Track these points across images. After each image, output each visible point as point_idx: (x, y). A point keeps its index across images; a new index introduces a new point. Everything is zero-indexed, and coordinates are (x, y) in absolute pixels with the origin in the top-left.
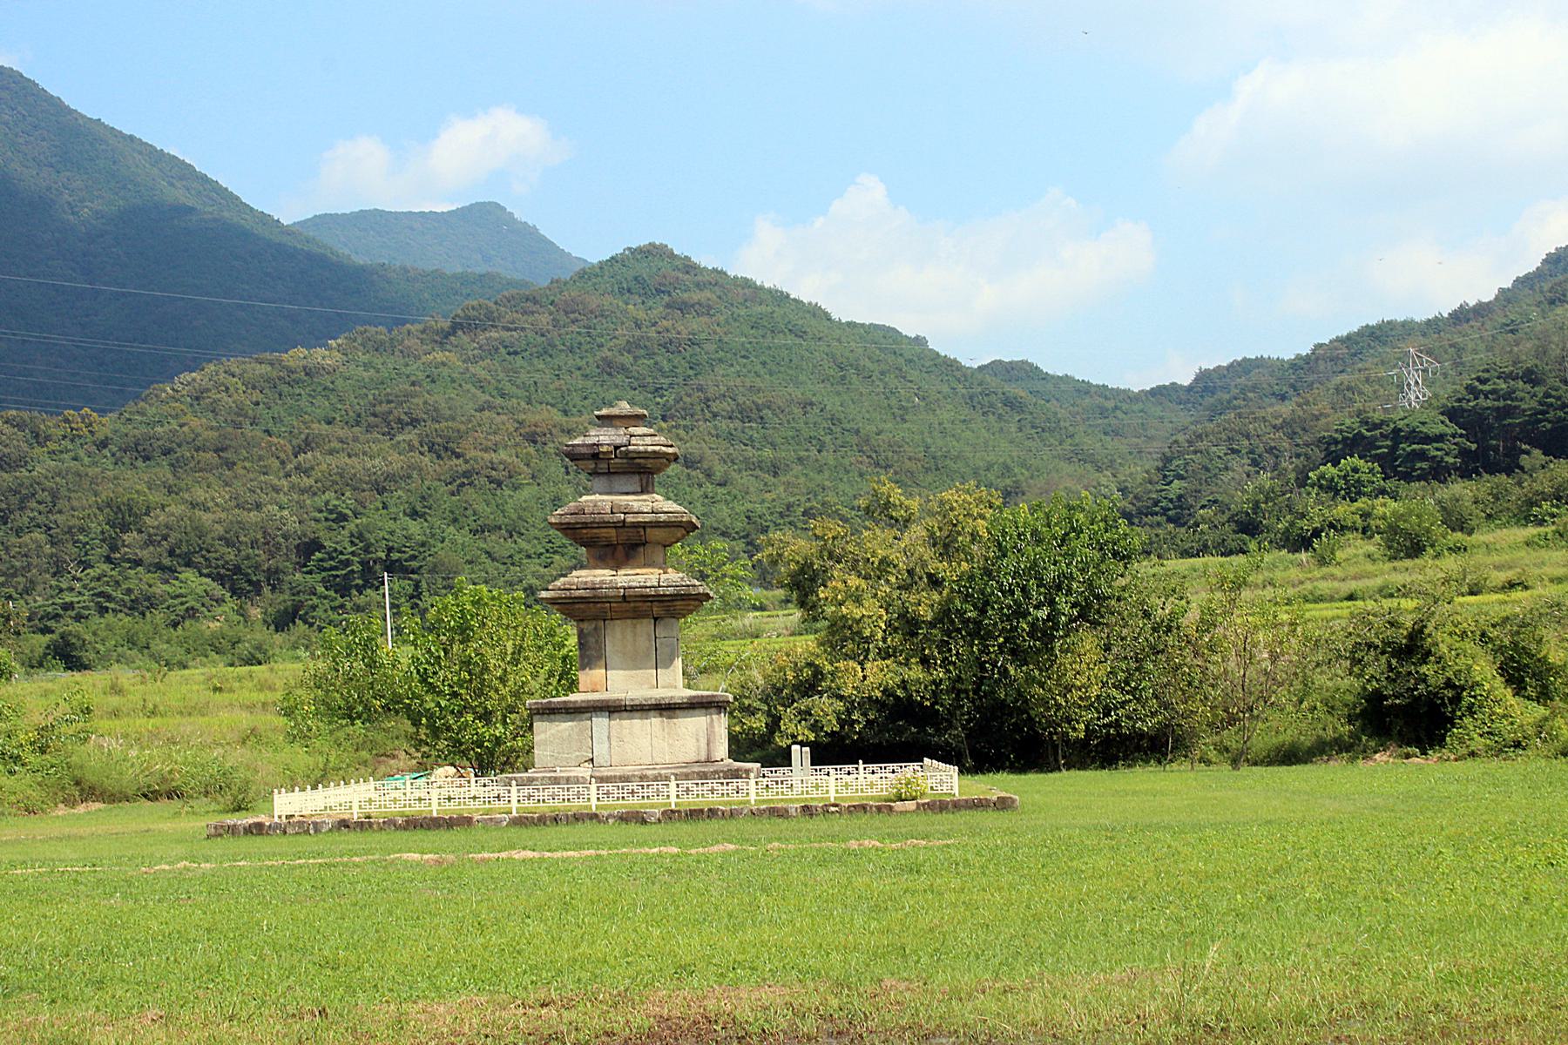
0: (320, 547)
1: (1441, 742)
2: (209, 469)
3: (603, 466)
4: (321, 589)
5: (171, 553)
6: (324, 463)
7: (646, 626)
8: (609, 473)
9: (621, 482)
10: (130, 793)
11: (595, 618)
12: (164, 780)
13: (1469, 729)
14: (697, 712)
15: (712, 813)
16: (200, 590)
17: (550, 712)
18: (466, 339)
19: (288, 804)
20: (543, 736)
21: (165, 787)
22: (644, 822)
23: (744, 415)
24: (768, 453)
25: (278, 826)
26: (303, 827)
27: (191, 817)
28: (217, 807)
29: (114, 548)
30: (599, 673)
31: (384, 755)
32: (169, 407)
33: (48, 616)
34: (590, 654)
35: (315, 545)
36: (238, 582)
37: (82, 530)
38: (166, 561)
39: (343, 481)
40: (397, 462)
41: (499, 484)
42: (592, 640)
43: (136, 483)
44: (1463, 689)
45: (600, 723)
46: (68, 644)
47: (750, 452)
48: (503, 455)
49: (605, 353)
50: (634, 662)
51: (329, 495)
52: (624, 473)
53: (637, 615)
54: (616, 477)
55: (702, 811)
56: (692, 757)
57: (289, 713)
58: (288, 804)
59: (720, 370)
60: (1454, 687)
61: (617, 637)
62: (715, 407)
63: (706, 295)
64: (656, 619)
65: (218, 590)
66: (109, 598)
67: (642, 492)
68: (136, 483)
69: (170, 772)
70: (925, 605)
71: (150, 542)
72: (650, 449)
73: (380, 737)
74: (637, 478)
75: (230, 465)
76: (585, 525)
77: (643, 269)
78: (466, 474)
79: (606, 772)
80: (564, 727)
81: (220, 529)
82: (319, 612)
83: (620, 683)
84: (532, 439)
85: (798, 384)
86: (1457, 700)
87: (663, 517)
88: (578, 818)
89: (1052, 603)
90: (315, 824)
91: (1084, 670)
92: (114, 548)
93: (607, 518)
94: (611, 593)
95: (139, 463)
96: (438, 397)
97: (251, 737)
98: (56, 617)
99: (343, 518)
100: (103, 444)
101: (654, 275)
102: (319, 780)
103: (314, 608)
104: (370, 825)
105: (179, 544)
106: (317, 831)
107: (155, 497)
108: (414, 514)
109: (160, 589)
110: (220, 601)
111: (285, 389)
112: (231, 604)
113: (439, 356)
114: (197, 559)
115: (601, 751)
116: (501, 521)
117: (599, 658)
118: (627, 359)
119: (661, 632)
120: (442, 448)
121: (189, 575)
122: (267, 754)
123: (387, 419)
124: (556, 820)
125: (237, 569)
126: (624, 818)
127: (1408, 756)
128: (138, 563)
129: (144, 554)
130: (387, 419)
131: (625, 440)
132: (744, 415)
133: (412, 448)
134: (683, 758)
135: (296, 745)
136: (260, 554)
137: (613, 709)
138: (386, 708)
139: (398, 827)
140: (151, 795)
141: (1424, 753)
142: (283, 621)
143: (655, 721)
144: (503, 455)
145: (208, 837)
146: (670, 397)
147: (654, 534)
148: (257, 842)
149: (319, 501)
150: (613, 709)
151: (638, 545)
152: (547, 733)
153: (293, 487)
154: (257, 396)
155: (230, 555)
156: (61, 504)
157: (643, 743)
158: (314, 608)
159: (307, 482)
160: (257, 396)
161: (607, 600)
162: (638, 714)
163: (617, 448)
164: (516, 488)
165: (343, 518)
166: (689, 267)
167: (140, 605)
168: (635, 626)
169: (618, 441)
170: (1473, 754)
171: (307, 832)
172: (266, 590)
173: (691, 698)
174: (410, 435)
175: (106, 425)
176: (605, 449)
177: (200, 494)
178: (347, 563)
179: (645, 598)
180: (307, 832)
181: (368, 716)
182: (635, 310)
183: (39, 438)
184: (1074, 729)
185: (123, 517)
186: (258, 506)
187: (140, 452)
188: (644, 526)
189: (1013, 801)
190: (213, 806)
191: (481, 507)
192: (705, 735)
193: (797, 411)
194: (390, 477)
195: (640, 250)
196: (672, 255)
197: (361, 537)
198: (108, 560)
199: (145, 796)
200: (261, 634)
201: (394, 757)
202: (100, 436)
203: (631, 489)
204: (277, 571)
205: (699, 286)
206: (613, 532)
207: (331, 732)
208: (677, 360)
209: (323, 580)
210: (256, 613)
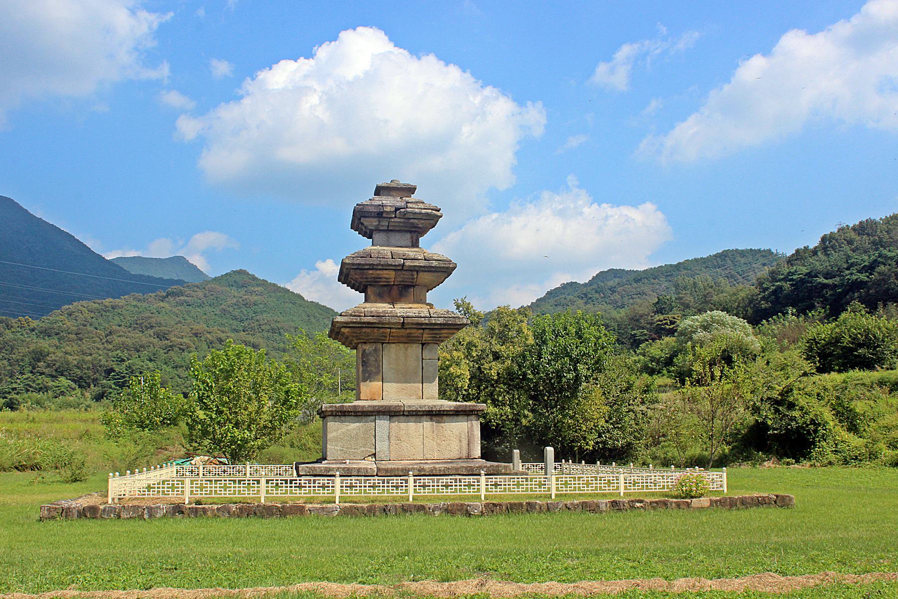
0: (114, 371)
1: (806, 456)
2: (73, 341)
3: (385, 223)
4: (113, 386)
5: (56, 371)
6: (117, 340)
7: (415, 350)
8: (388, 231)
9: (396, 237)
10: (6, 466)
11: (376, 341)
12: (29, 458)
13: (826, 447)
14: (460, 418)
15: (531, 507)
16: (66, 385)
17: (342, 414)
18: (172, 299)
19: (122, 487)
20: (334, 434)
21: (29, 463)
22: (469, 514)
23: (273, 331)
24: (282, 345)
25: (112, 510)
26: (137, 512)
27: (41, 486)
28: (58, 478)
29: (34, 368)
30: (376, 385)
31: (161, 448)
32: (57, 318)
33: (6, 392)
34: (369, 369)
35: (112, 370)
36: (82, 383)
37: (22, 360)
38: (54, 373)
39: (124, 347)
40: (145, 340)
41: (183, 350)
42: (372, 359)
43: (45, 344)
44: (819, 424)
45: (382, 424)
46: (12, 403)
47: (275, 344)
48: (185, 340)
49: (223, 306)
50: (404, 377)
51: (118, 352)
52: (399, 231)
53: (409, 340)
54: (393, 234)
55: (521, 504)
56: (455, 454)
57: (108, 423)
58: (122, 487)
59: (265, 315)
60: (815, 424)
61: (392, 356)
62: (263, 327)
63: (260, 289)
64: (423, 344)
65: (73, 385)
66: (31, 387)
67: (413, 246)
68: (45, 344)
69: (34, 454)
70: (494, 369)
71: (48, 366)
72: (424, 211)
73: (158, 438)
74: (408, 236)
75: (81, 340)
76: (373, 267)
77: (238, 278)
78: (171, 346)
79: (384, 465)
80: (353, 426)
81: (76, 362)
82: (112, 395)
83: (393, 394)
84: (196, 335)
85: (293, 321)
86: (816, 431)
87: (435, 263)
88: (405, 509)
89: (575, 369)
90: (150, 509)
91: (593, 407)
92: (34, 368)
93: (390, 261)
94: (393, 320)
95: (46, 338)
96: (160, 318)
97: (86, 435)
98: (9, 393)
99: (123, 360)
100: (33, 330)
101: (240, 280)
102: (131, 466)
103: (110, 393)
104: (205, 511)
105: (59, 367)
106: (151, 516)
107: (52, 350)
108: (151, 360)
109: (51, 384)
110: (74, 389)
111: (104, 313)
112: (78, 390)
113: (162, 304)
114: (66, 373)
115: (382, 447)
116: (183, 364)
117: (377, 373)
118: (231, 309)
119: (426, 354)
120: (161, 336)
121: (62, 379)
122: (94, 445)
123: (141, 326)
124: (385, 510)
125: (81, 378)
126: (449, 511)
127: (788, 464)
128: (41, 374)
129: (46, 371)
130: (141, 326)
131: (403, 204)
132: (273, 331)
133: (150, 336)
134: (448, 455)
135: (110, 441)
136: (90, 373)
137: (393, 413)
138: (162, 422)
139: (231, 514)
140: (20, 468)
141: (797, 462)
142: (99, 398)
143: (427, 425)
144: (185, 340)
145: (41, 520)
146: (246, 324)
147: (425, 277)
148: (91, 526)
149: (114, 353)
150: (393, 413)
151: (409, 286)
152: (339, 431)
153: (105, 348)
154: (92, 315)
155: (79, 372)
156: (15, 351)
157: (420, 442)
158: (110, 393)
159: (110, 346)
160: (92, 315)
161: (390, 326)
162: (414, 418)
163: (397, 209)
164: (189, 352)
165: (123, 360)
166: (254, 278)
167: (44, 389)
168: (406, 349)
169: (398, 204)
170: (830, 463)
171: (141, 517)
172: (92, 386)
173: (456, 407)
174: (151, 332)
175: (34, 324)
176: (388, 209)
177: (69, 349)
178: (124, 377)
179: (420, 326)
180: (141, 517)
181: (153, 426)
182: (234, 291)
183: (9, 327)
184: (587, 444)
185: (39, 356)
186: (91, 355)
187: (46, 333)
188: (417, 270)
189: (791, 499)
190: (58, 478)
191: (176, 359)
192: (462, 437)
193: (293, 330)
194: (142, 346)
195: (236, 271)
196: (248, 274)
197: (130, 367)
198: (31, 372)
199: (17, 468)
200: (89, 402)
201: (166, 450)
202: (32, 327)
203: (404, 243)
204: (97, 379)
205: (258, 285)
206: (392, 274)
207: (131, 435)
208: (249, 310)
209: (114, 384)
210: (88, 394)
